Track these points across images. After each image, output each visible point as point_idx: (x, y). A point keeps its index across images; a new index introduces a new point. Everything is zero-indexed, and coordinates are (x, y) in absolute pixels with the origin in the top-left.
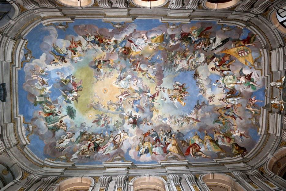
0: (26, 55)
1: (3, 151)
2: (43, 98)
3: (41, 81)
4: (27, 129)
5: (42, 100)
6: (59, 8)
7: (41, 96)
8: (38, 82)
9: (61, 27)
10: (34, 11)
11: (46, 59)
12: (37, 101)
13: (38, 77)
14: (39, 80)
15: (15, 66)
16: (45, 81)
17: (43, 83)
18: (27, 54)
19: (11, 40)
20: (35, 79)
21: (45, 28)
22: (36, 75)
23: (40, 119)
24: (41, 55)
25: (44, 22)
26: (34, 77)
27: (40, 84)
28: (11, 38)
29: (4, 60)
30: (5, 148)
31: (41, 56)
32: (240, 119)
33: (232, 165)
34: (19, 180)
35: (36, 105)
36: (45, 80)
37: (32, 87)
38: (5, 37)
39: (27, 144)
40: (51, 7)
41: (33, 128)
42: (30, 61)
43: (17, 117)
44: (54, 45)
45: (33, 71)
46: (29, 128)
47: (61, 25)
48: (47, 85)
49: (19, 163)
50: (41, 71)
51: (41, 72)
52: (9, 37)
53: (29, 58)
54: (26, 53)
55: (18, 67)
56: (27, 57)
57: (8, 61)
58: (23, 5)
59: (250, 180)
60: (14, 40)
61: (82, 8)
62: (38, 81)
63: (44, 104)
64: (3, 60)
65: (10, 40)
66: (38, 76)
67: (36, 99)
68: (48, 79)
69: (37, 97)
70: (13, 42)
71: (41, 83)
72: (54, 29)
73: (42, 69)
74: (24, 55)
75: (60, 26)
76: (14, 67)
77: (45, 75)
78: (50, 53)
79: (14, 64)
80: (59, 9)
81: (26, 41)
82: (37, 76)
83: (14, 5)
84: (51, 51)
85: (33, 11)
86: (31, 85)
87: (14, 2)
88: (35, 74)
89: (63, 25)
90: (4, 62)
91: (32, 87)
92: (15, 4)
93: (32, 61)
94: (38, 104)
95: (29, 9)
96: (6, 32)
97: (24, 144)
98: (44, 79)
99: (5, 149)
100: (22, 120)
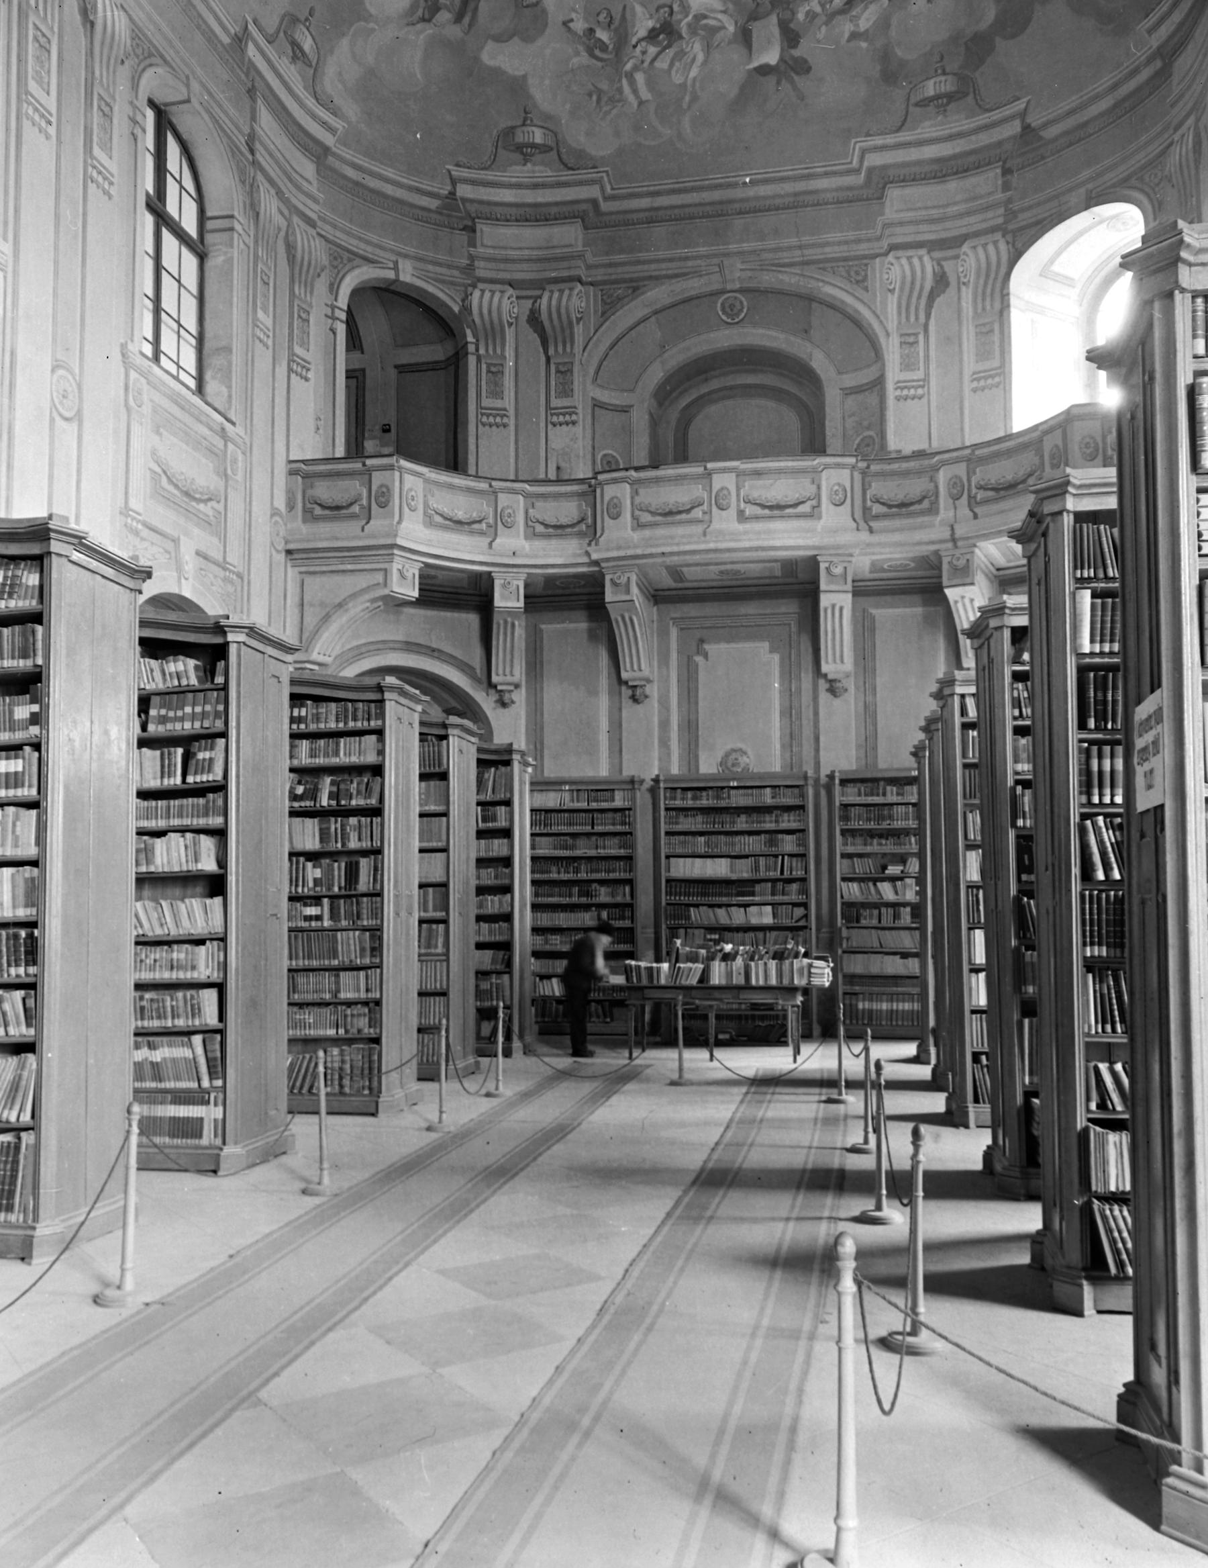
0: (526, 152)
1: (1008, 243)
2: (756, 28)
3: (652, 50)
4: (942, 105)
5: (776, 31)
6: (250, 157)
7: (745, 37)
8: (662, 64)
9: (307, 45)
10: (314, 216)
11: (516, 39)
12: (782, 59)
13: (636, 68)
14: (648, 59)
15: (594, 202)
16: (650, 24)
17: (665, 33)
18: (519, 148)
19: (479, 243)
20: (650, 84)
21: (352, 110)
22: (625, 82)
23: (893, 33)
24: (497, 72)
25: (329, 140)
26: (635, 91)
27: (670, 53)
28: (472, 243)
29: (581, 256)
30: (998, 236)
31: (504, 73)
32: (598, 1307)
33: (954, 130)
34: (1155, 219)
35: (806, 61)
36: (643, 24)
37: (695, 98)
38: (480, 273)
39: (1023, 115)
40: (267, 185)
41: (944, 73)
42: (549, 123)
43: (857, 171)
44: (415, 18)
45: (605, 99)
46: (937, 97)
47: (297, 54)
48: (676, 7)
49: (1090, 186)
50: (592, 55)
51: (597, 52)
52: (472, 258)
53: (538, 137)
54: (517, 156)
55: (597, 187)
56: (534, 146)
57: (581, 237)
58: (323, 275)
59: (928, 316)
60: (474, 231)
61: (187, 77)
62: (657, 64)
63: (801, 16)
64: (580, 263)
65: (482, 245)
66: (628, 67)
67: (764, 70)
68: (639, 9)
69: (755, 64)
70: (486, 229)
71: (669, 46)
72: (330, 71)
73: (581, 48)
74: (529, 165)
75: (302, 51)
76: (605, 206)
77: (616, 30)
78: (470, 25)
79: (584, 206)
80: (252, 152)
81: (457, 172)
82: (630, 76)
83: (343, 302)
84: (458, 19)
85: (319, 223)
86: (685, 106)
87: (333, 307)
88: (620, 90)
89: (295, 45)
90: (590, 259)
91: (695, 98)
92: (336, 300)
93: (548, 117)
94: (796, 53)
95: (324, 242)
96: (456, 273)
97: (1019, 129)
98: (642, 33)
99: (1004, 236)
100: (879, 141)
